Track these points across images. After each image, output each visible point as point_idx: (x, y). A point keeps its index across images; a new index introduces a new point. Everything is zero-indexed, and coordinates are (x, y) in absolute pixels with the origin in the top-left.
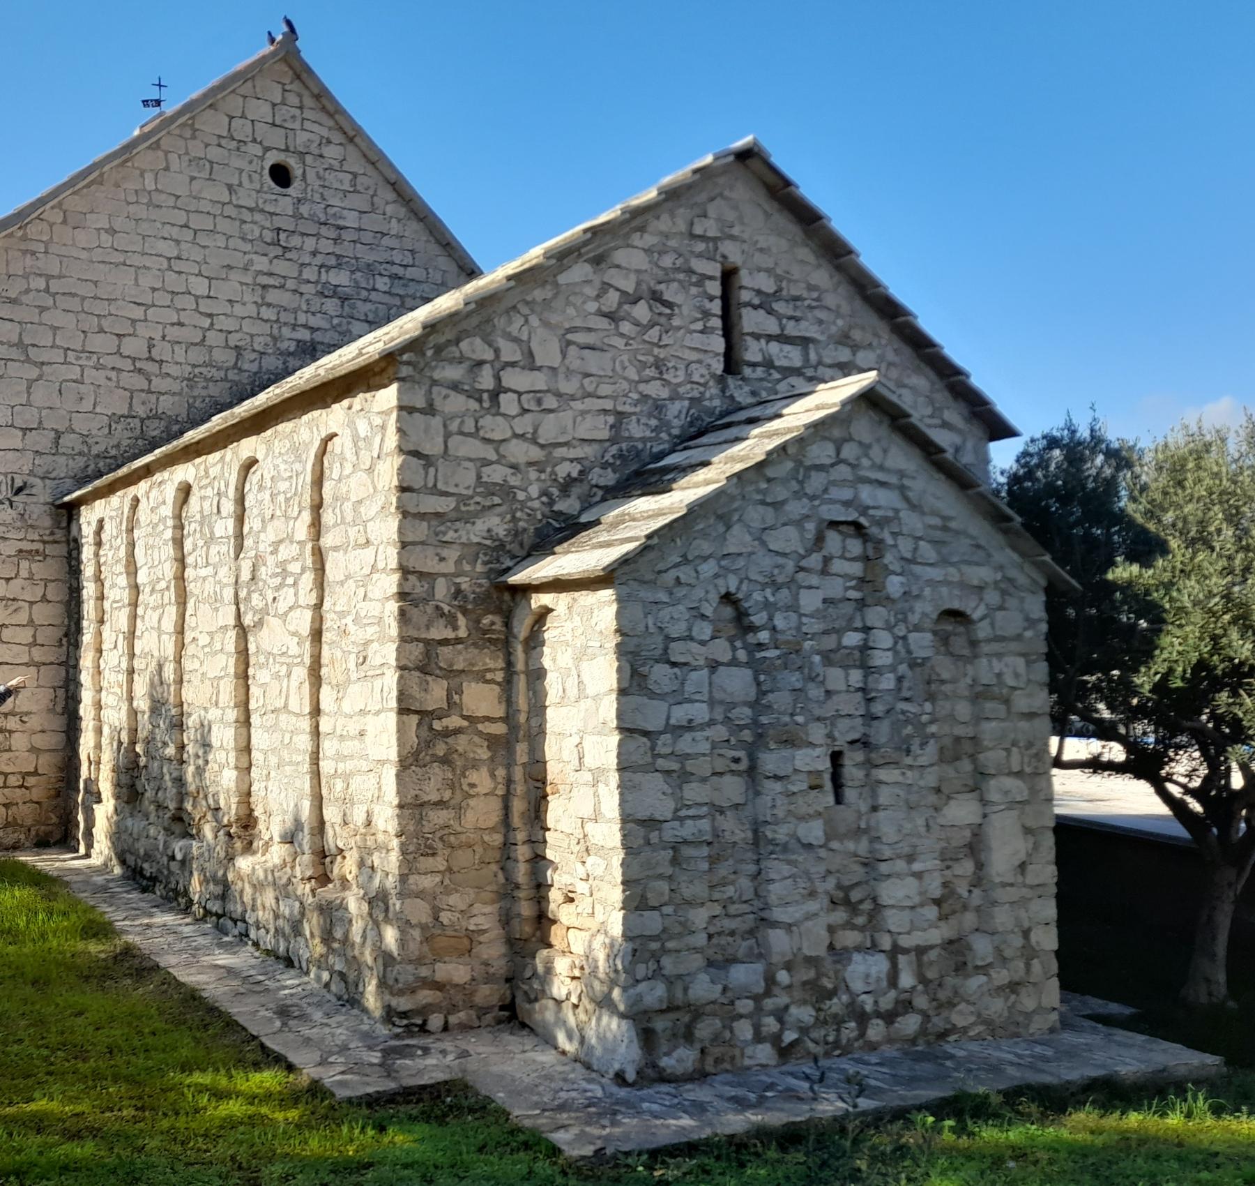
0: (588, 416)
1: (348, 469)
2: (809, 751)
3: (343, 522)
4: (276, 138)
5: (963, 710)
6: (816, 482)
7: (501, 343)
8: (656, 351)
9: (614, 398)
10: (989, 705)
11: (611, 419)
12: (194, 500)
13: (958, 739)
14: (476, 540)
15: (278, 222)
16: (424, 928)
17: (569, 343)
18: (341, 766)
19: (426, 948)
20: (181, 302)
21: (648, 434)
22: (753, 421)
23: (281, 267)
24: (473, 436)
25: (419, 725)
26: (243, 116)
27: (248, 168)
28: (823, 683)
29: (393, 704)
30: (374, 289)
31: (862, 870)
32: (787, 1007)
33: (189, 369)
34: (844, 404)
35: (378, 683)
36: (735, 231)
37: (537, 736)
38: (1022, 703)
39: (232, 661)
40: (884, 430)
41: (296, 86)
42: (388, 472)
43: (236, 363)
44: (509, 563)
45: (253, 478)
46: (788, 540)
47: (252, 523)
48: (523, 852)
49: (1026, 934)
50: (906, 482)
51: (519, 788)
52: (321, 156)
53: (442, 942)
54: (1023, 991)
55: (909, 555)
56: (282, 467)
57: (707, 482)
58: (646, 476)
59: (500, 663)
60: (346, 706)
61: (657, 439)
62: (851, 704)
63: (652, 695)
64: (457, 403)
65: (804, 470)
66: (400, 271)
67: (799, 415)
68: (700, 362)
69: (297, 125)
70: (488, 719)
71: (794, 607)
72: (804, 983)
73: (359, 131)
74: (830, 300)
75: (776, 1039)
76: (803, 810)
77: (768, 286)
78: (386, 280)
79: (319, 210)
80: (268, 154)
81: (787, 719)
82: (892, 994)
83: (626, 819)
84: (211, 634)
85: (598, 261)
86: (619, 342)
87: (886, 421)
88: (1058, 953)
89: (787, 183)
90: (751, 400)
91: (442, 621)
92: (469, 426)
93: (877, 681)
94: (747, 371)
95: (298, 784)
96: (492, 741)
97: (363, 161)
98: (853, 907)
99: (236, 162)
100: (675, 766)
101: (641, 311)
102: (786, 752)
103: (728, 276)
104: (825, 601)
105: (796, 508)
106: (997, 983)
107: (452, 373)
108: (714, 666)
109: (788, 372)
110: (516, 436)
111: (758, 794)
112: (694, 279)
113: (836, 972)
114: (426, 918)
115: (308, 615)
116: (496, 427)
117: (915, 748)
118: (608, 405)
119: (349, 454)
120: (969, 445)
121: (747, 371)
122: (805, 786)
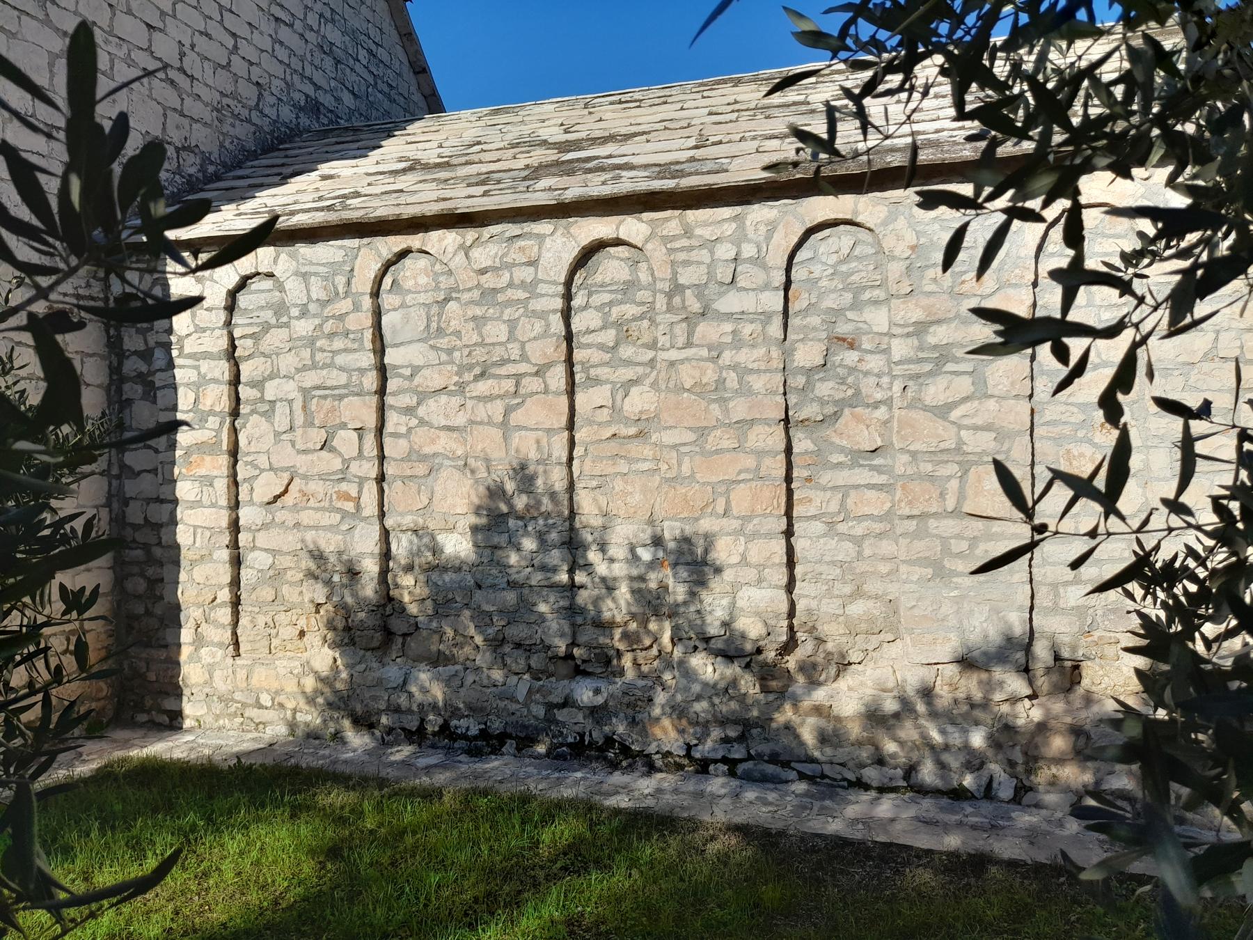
25: (56, 498)
43: (258, 104)
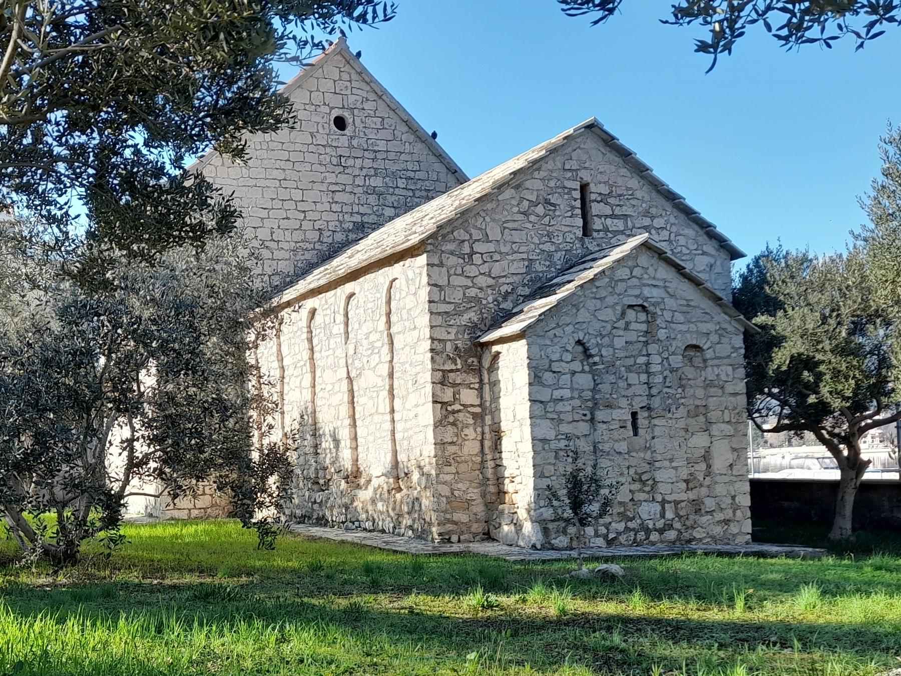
0: (515, 263)
1: (404, 294)
2: (619, 410)
3: (402, 320)
4: (336, 101)
5: (700, 393)
6: (621, 287)
7: (473, 231)
8: (548, 228)
9: (528, 253)
10: (712, 390)
11: (526, 263)
12: (317, 316)
13: (697, 406)
14: (464, 323)
15: (340, 152)
16: (447, 497)
17: (505, 228)
18: (406, 434)
19: (448, 506)
20: (287, 205)
21: (545, 269)
22: (594, 260)
23: (343, 179)
24: (462, 275)
26: (318, 90)
27: (322, 121)
28: (627, 379)
29: (431, 399)
30: (397, 187)
31: (648, 466)
32: (610, 523)
33: (294, 244)
34: (632, 250)
35: (423, 391)
36: (587, 165)
37: (495, 411)
38: (729, 388)
39: (346, 396)
40: (655, 261)
41: (347, 68)
42: (424, 294)
44: (480, 334)
45: (353, 302)
46: (608, 315)
47: (353, 325)
48: (490, 464)
49: (733, 498)
50: (667, 284)
51: (487, 436)
52: (363, 109)
53: (455, 504)
54: (732, 524)
55: (670, 320)
56: (370, 296)
57: (567, 290)
58: (543, 289)
59: (477, 380)
60: (408, 406)
61: (550, 271)
62: (642, 390)
63: (544, 385)
64: (453, 261)
65: (614, 282)
66: (412, 174)
67: (616, 254)
68: (570, 232)
69: (349, 92)
70: (472, 406)
71: (611, 346)
72: (619, 514)
73: (385, 92)
74: (638, 194)
75: (605, 537)
76: (616, 437)
77: (605, 190)
78: (404, 180)
79: (363, 141)
80: (333, 111)
81: (608, 396)
82: (663, 521)
83: (533, 439)
84: (333, 384)
85: (517, 187)
86: (530, 226)
87: (656, 256)
88: (750, 507)
89: (613, 138)
90: (597, 249)
91: (450, 361)
92: (459, 271)
93: (653, 379)
94: (595, 234)
95: (385, 446)
96: (475, 416)
97: (388, 109)
98: (644, 483)
99: (315, 118)
100: (556, 417)
101: (540, 210)
102: (609, 411)
103: (584, 188)
104: (626, 342)
105: (611, 300)
106: (717, 519)
107: (450, 247)
108: (574, 373)
109: (616, 233)
110: (481, 274)
111: (595, 430)
112: (566, 191)
113: (634, 509)
114: (448, 494)
115: (387, 366)
116: (471, 271)
117: (673, 409)
118: (525, 256)
119: (404, 287)
120: (718, 263)
121: (595, 234)
122: (618, 426)
